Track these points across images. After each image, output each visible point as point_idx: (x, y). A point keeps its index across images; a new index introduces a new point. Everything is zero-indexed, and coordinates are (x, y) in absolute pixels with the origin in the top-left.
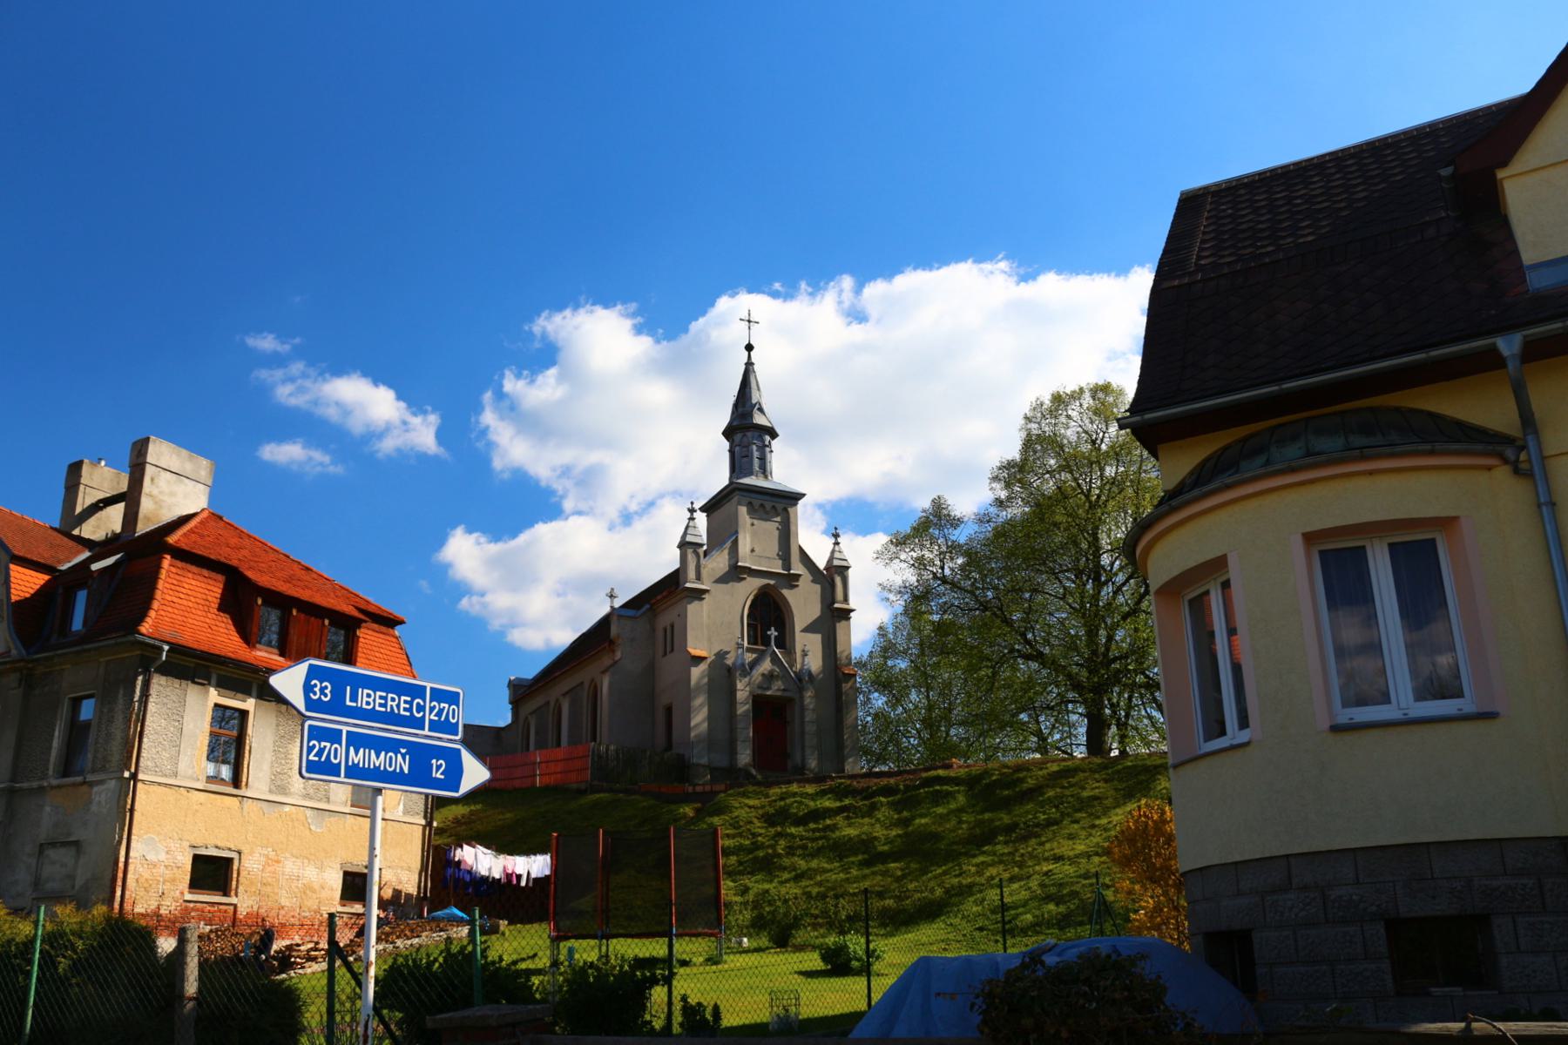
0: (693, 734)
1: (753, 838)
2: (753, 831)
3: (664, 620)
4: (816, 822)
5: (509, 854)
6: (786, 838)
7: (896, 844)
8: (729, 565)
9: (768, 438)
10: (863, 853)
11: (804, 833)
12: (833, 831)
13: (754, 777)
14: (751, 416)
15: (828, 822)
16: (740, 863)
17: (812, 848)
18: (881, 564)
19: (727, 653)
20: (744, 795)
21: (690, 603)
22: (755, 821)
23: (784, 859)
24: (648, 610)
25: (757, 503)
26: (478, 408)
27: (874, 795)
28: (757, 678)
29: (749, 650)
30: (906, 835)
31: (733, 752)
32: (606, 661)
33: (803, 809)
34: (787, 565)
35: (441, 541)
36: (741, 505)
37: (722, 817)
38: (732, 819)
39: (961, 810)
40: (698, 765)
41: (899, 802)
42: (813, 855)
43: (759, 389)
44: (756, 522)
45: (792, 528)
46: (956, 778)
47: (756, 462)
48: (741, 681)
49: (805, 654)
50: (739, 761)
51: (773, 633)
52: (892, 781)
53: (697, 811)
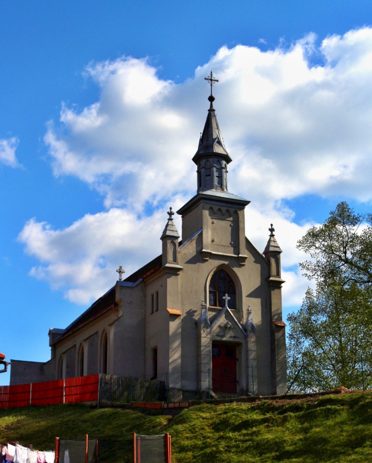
1: (204, 440)
2: (204, 435)
3: (151, 289)
4: (246, 429)
5: (39, 450)
6: (226, 440)
7: (298, 445)
8: (197, 252)
9: (224, 162)
10: (276, 451)
11: (238, 437)
12: (257, 436)
13: (212, 397)
14: (212, 146)
15: (254, 429)
16: (194, 457)
17: (243, 447)
18: (303, 250)
19: (195, 311)
20: (200, 410)
21: (169, 277)
22: (207, 428)
23: (224, 454)
24: (141, 282)
25: (216, 208)
26: (44, 131)
27: (285, 411)
28: (216, 329)
29: (210, 310)
30: (306, 439)
31: (198, 380)
32: (113, 317)
33: (239, 420)
34: (237, 250)
35: (20, 228)
36: (205, 209)
37: (184, 425)
38: (191, 426)
39: (343, 423)
40: (173, 389)
41: (303, 416)
42: (243, 452)
43: (218, 128)
44: (215, 221)
45: (241, 225)
46: (342, 400)
47: (216, 180)
49: (249, 313)
50: (202, 386)
51: (227, 298)
52: (299, 401)
53: (170, 420)
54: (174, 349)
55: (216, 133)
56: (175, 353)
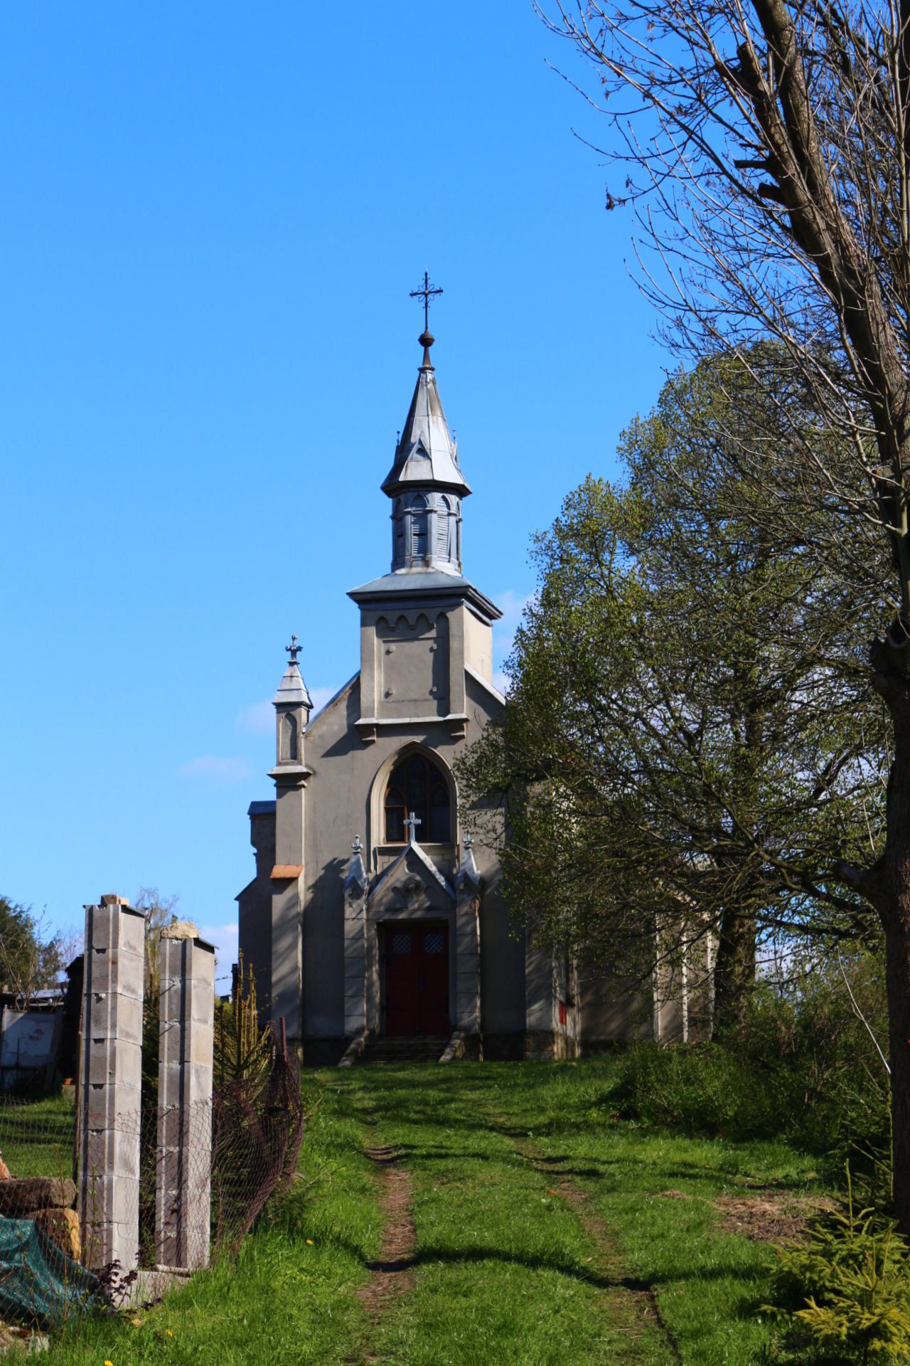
0: (275, 993)
19: (344, 862)
25: (392, 617)
44: (393, 647)
45: (454, 644)
48: (351, 906)
54: (282, 954)
55: (421, 427)
56: (283, 962)
